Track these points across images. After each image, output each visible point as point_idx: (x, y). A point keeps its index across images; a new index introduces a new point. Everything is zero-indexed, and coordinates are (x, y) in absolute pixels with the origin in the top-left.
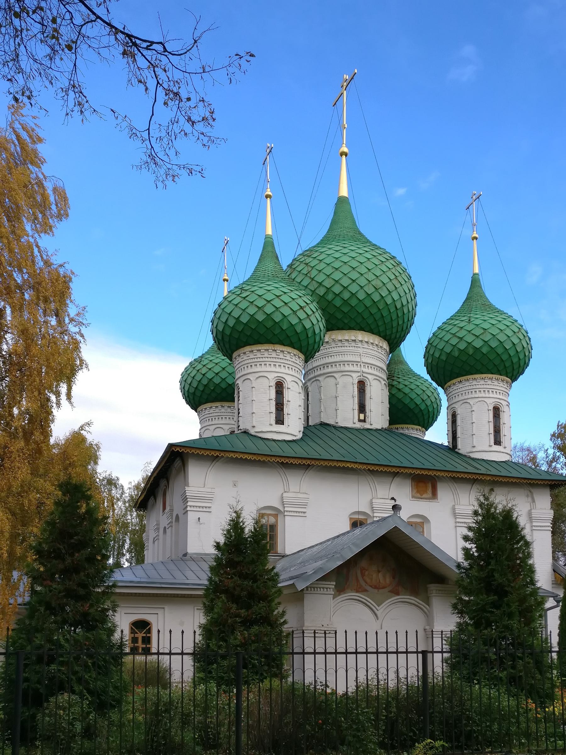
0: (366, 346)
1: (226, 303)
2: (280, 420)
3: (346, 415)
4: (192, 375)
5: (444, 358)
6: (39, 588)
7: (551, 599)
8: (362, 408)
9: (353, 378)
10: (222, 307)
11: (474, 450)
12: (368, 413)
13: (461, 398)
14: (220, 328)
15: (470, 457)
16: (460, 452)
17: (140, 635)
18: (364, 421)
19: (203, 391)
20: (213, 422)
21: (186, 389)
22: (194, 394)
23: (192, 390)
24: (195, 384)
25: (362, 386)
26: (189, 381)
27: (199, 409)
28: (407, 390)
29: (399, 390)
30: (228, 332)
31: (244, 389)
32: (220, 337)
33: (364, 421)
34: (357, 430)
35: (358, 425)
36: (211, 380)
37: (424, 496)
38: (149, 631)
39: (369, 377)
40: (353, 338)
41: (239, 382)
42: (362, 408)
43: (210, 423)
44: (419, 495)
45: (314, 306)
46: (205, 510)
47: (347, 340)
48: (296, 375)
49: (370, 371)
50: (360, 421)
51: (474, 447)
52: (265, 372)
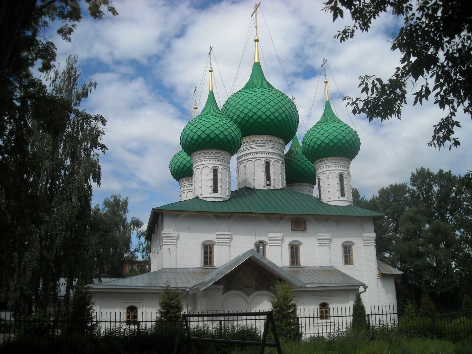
0: (269, 143)
1: (187, 129)
2: (215, 190)
3: (259, 182)
4: (175, 162)
5: (310, 149)
6: (387, 255)
7: (361, 287)
8: (268, 178)
9: (257, 164)
10: (185, 131)
11: (330, 200)
12: (272, 180)
13: (322, 170)
14: (184, 142)
15: (328, 205)
16: (323, 201)
17: (132, 314)
18: (270, 185)
19: (181, 171)
20: (187, 189)
21: (172, 170)
22: (176, 173)
23: (175, 171)
24: (176, 168)
25: (267, 165)
26: (173, 166)
27: (180, 181)
28: (299, 163)
29: (295, 163)
30: (187, 144)
31: (197, 173)
32: (184, 146)
33: (270, 185)
34: (267, 190)
35: (267, 188)
36: (185, 165)
37: (300, 229)
38: (136, 312)
39: (273, 160)
40: (262, 139)
41: (194, 170)
42: (268, 178)
43: (185, 189)
44: (296, 229)
45: (235, 126)
46: (172, 243)
47: (258, 140)
48: (225, 164)
49: (272, 156)
50: (267, 185)
51: (330, 198)
52: (204, 166)
